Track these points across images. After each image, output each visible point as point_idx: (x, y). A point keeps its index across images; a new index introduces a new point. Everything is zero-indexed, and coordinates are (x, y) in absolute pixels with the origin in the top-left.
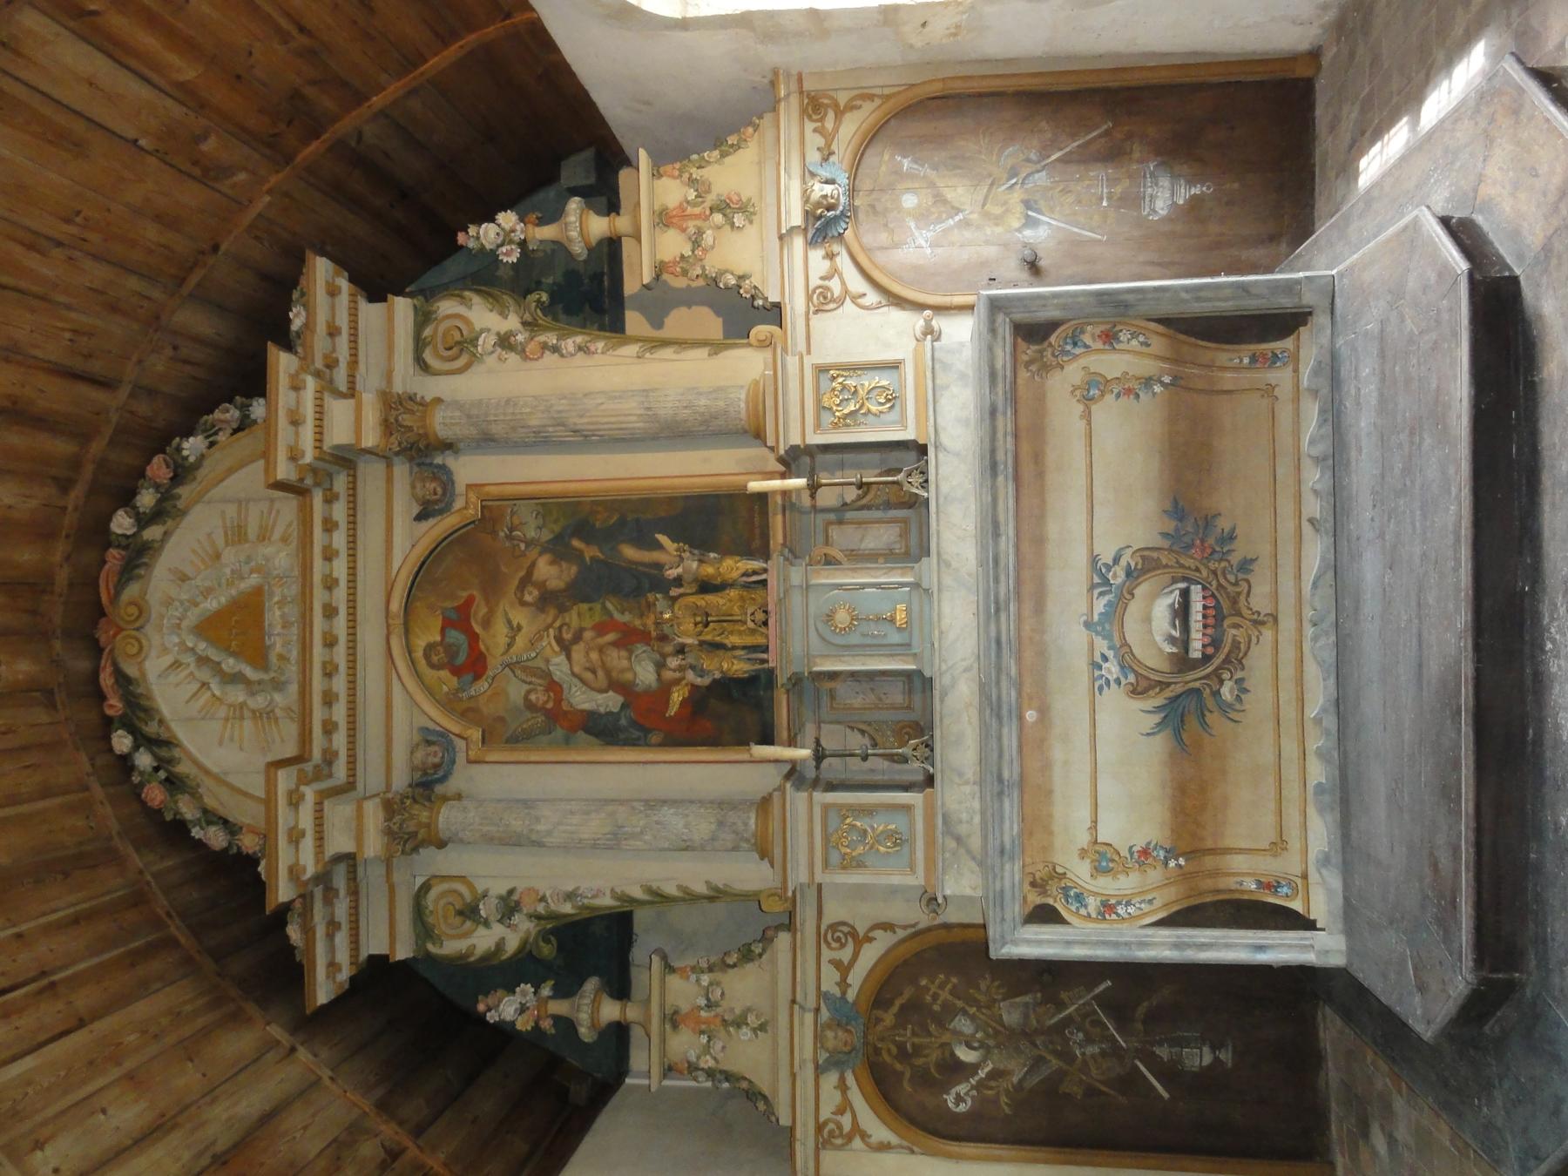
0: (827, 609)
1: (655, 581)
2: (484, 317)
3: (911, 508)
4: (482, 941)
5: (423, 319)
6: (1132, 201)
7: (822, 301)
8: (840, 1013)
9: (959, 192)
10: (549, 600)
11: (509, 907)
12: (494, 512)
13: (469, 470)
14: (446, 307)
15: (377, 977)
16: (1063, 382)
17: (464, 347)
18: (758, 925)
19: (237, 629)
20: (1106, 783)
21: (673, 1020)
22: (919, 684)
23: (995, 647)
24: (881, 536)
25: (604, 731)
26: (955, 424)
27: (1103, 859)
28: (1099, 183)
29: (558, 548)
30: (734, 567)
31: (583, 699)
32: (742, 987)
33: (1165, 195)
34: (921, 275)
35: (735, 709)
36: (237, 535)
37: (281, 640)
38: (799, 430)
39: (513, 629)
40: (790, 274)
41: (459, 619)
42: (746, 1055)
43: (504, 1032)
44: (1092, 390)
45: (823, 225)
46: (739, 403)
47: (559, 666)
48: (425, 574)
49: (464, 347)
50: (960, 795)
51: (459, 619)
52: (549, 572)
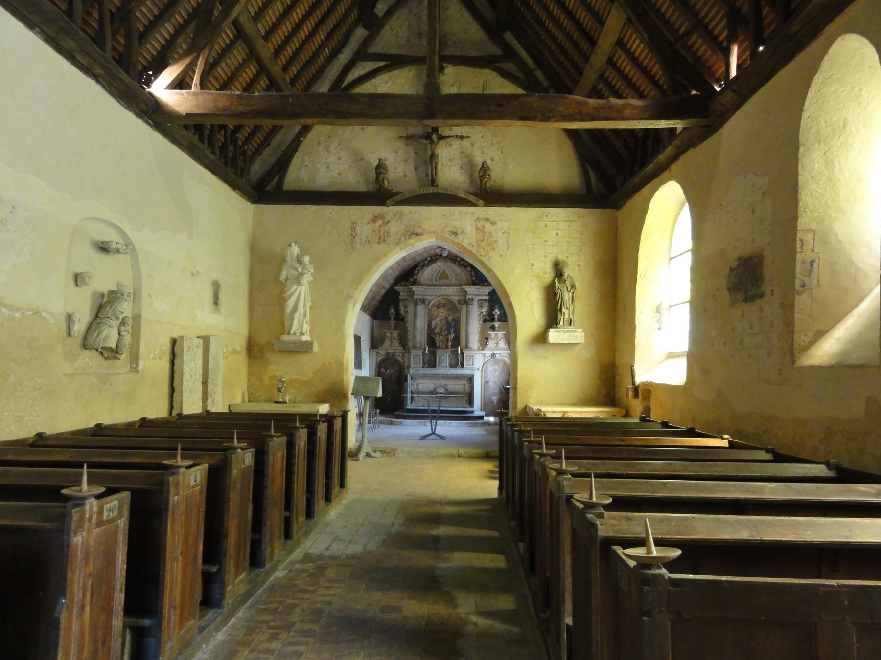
0: (444, 356)
1: (449, 334)
2: (485, 310)
3: (453, 366)
4: (402, 308)
5: (486, 300)
6: (495, 395)
7: (484, 355)
8: (394, 355)
9: (497, 373)
10: (446, 318)
11: (406, 312)
12: (458, 311)
13: (464, 307)
14: (487, 304)
15: (398, 293)
16: (465, 382)
17: (481, 307)
18: (403, 341)
19: (444, 275)
20: (425, 385)
21: (391, 333)
22: (434, 366)
23: (456, 524)
24: (453, 362)
25: (429, 325)
26: (465, 371)
27: (417, 385)
28: (497, 391)
29: (453, 320)
30: (450, 344)
31: (433, 323)
32: (396, 343)
33: (495, 399)
34: (487, 368)
35: (432, 343)
36: (457, 275)
37: (442, 282)
38: (466, 353)
39: (443, 313)
40: (488, 352)
41: (444, 305)
42: (387, 343)
43: (389, 310)
44: (465, 385)
45: (493, 355)
46: (471, 345)
47: (438, 319)
48: (451, 301)
49: (481, 307)
50: (422, 371)
51: (444, 305)
52: (451, 318)
